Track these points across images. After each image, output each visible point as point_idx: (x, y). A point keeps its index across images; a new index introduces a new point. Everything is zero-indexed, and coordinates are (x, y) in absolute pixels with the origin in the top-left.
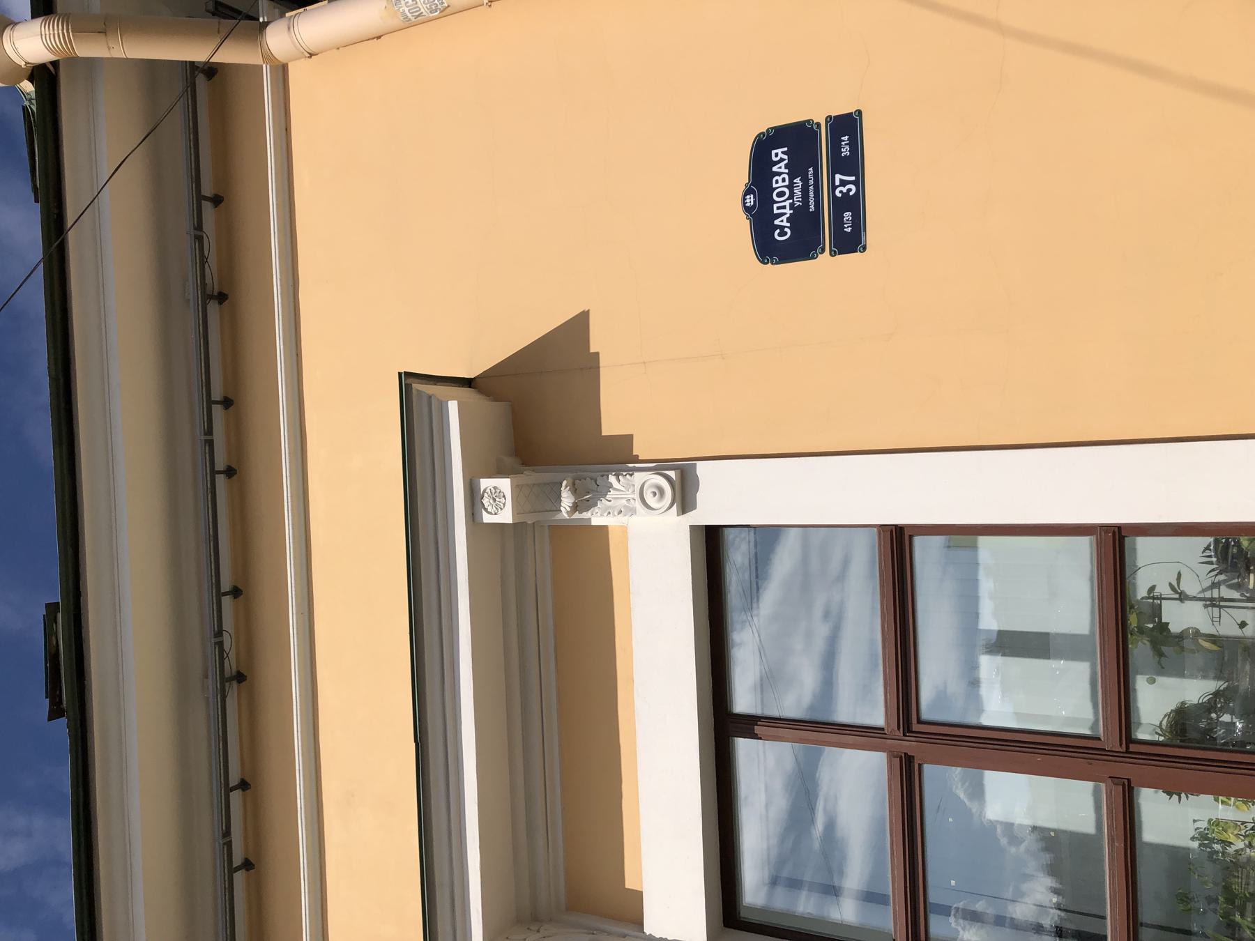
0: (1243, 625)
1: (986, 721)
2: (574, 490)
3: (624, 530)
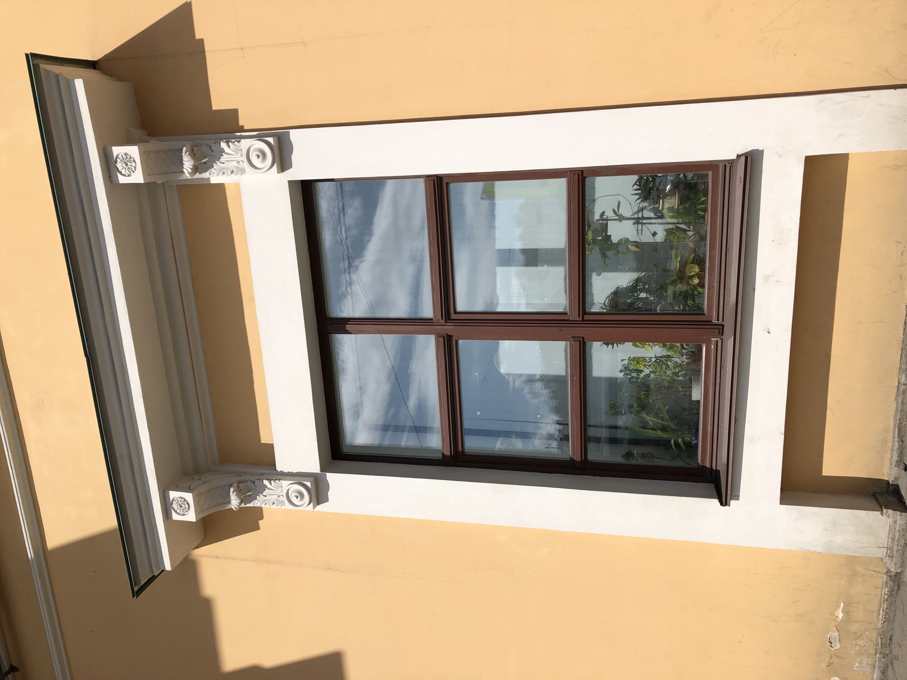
0: (654, 234)
1: (499, 309)
2: (193, 155)
3: (237, 186)
